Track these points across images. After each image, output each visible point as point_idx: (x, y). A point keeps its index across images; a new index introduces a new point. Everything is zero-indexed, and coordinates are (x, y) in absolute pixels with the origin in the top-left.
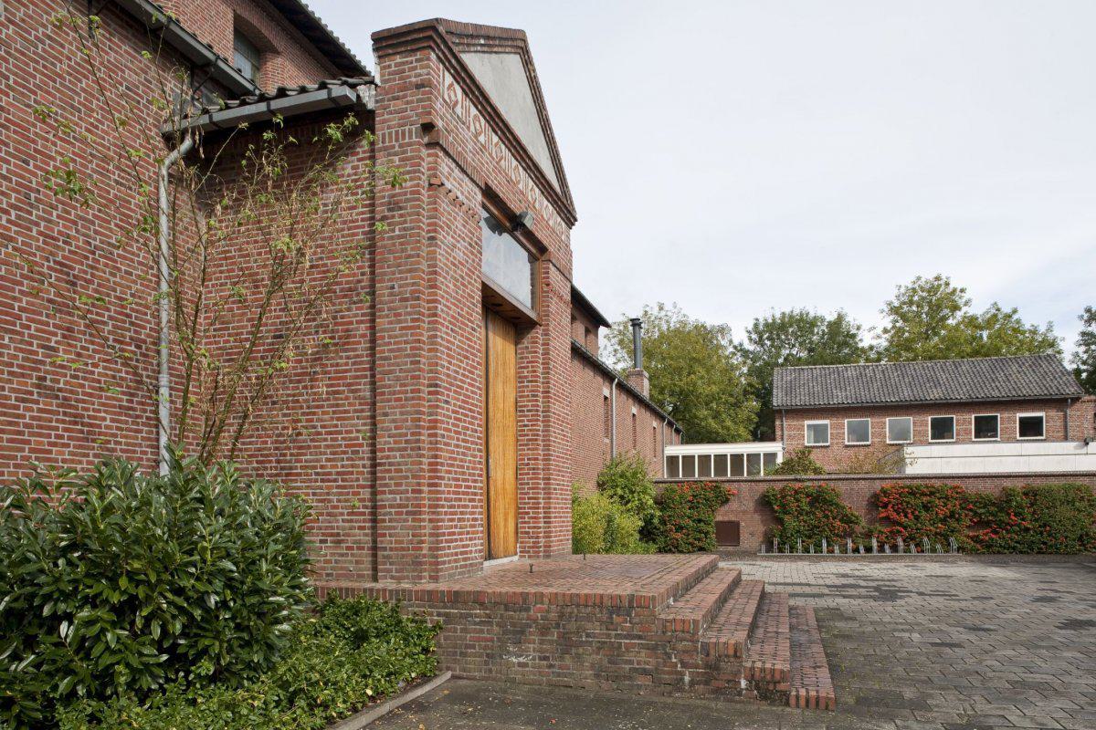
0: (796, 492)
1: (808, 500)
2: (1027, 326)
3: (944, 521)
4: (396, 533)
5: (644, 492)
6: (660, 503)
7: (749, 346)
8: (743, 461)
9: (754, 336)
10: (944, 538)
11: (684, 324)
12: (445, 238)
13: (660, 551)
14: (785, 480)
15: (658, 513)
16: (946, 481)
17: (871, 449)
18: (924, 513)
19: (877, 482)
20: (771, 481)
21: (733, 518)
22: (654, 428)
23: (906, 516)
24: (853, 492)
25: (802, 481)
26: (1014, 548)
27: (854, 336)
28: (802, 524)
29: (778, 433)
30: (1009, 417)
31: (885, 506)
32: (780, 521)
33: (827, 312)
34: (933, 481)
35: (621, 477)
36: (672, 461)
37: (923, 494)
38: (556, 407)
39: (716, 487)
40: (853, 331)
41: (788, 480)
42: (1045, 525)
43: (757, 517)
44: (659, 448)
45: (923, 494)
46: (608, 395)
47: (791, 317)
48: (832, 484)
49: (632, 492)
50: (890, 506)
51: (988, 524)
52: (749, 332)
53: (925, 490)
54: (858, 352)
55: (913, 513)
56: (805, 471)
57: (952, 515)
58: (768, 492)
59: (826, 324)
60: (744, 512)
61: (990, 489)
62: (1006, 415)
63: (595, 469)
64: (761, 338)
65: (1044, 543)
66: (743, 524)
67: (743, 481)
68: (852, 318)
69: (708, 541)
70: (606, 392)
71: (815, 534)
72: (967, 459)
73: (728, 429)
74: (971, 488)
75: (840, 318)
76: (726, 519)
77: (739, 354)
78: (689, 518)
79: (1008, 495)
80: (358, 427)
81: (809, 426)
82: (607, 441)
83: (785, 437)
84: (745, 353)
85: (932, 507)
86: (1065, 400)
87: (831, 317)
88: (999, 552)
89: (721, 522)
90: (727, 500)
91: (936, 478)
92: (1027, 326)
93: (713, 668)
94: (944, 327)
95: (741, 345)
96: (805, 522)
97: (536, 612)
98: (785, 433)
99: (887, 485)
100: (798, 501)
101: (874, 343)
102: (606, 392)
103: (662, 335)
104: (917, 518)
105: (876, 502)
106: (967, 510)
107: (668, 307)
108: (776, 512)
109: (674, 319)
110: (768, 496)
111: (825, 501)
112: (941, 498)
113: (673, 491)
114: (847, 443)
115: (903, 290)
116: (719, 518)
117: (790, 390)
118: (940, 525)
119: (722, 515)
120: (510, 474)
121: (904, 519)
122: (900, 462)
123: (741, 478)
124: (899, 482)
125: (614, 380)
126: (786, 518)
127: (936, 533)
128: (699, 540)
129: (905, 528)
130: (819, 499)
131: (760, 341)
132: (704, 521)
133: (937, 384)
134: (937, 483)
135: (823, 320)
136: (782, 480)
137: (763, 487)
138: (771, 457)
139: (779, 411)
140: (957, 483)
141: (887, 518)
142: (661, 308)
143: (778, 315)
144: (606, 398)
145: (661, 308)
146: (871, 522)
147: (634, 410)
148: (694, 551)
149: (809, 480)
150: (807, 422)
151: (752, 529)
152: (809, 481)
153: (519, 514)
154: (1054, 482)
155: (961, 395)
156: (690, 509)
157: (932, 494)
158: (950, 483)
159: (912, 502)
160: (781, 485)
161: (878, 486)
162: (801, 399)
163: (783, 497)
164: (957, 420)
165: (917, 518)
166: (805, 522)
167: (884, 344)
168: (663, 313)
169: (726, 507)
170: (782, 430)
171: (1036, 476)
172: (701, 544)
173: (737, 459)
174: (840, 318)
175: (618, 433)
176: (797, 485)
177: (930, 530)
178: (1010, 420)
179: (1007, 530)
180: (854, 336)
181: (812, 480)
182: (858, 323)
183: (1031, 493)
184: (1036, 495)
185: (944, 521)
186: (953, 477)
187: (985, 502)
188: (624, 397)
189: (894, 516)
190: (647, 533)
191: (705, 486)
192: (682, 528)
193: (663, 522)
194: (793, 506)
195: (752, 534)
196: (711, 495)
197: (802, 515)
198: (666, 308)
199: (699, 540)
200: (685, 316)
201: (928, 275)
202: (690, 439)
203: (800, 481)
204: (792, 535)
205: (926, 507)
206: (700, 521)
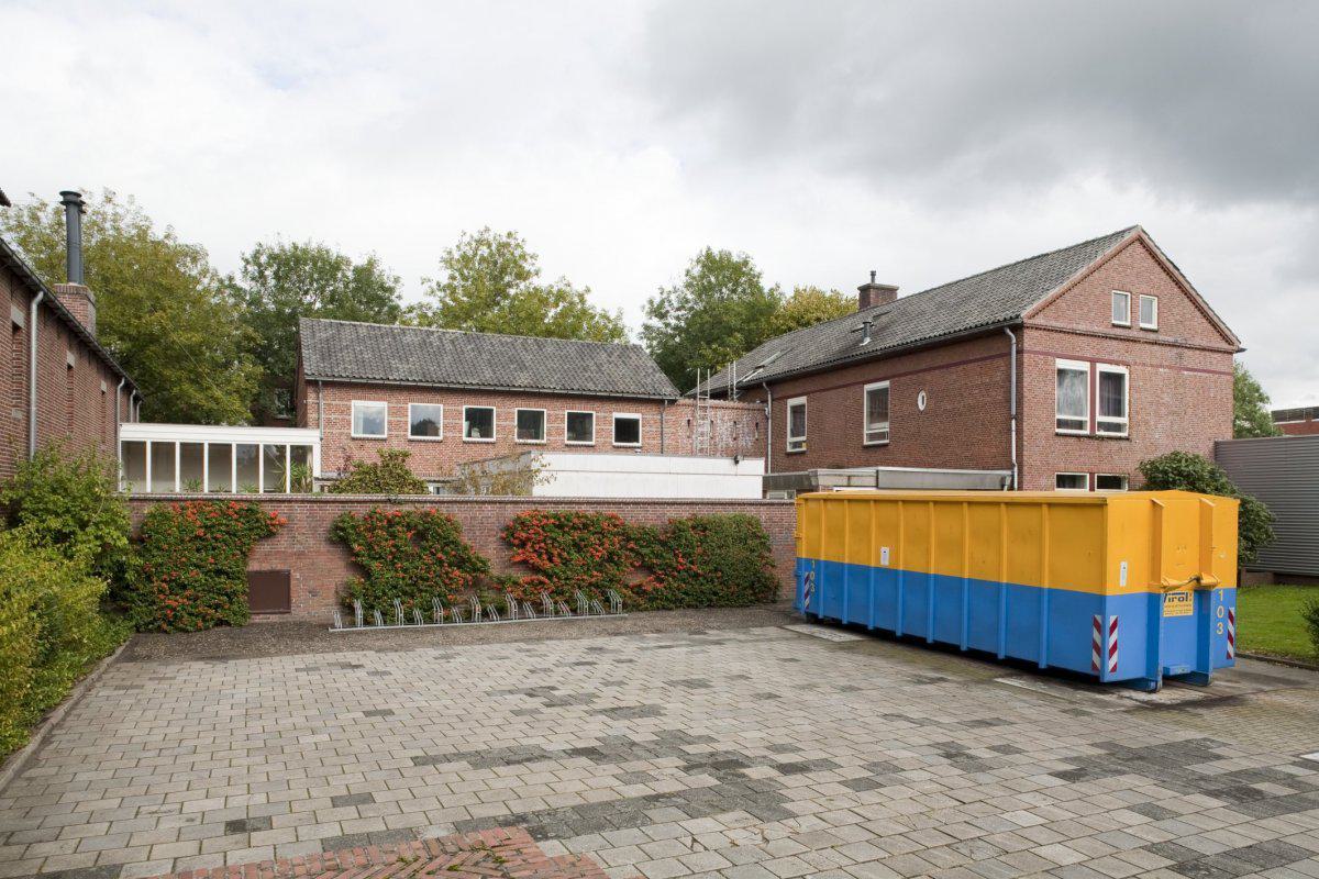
0: (391, 523)
1: (409, 535)
2: (599, 310)
3: (600, 567)
6: (140, 540)
7: (240, 282)
8: (202, 450)
9: (252, 268)
10: (600, 591)
11: (143, 233)
14: (371, 501)
16: (599, 508)
17: (442, 446)
18: (575, 556)
20: (347, 502)
21: (277, 565)
22: (103, 393)
23: (551, 560)
24: (475, 523)
25: (400, 503)
26: (681, 601)
27: (391, 290)
28: (401, 574)
29: (312, 416)
30: (605, 417)
31: (523, 544)
33: (353, 250)
34: (584, 507)
35: (54, 491)
37: (574, 528)
39: (249, 511)
40: (389, 284)
41: (377, 502)
42: (716, 570)
44: (110, 427)
45: (574, 528)
46: (21, 323)
47: (305, 251)
48: (444, 509)
49: (83, 525)
50: (530, 544)
52: (247, 262)
53: (576, 520)
54: (394, 314)
55: (559, 555)
57: (610, 558)
58: (343, 521)
59: (351, 268)
61: (649, 519)
62: (601, 414)
64: (261, 274)
65: (715, 594)
66: (296, 575)
67: (283, 501)
68: (387, 269)
69: (235, 607)
70: (17, 315)
71: (421, 591)
72: (609, 475)
73: (217, 401)
74: (632, 518)
75: (371, 263)
76: (266, 567)
77: (227, 291)
78: (197, 566)
79: (676, 530)
82: (20, 415)
83: (322, 423)
84: (238, 292)
85: (585, 546)
86: (662, 401)
87: (358, 260)
88: (664, 608)
89: (257, 572)
90: (270, 535)
91: (588, 503)
92: (599, 310)
94: (506, 296)
95: (231, 279)
96: (405, 571)
99: (523, 511)
100: (393, 536)
101: (425, 300)
102: (17, 315)
103: (104, 244)
104: (566, 562)
106: (627, 549)
107: (120, 199)
108: (357, 555)
109: (128, 220)
110: (343, 529)
112: (596, 533)
113: (165, 517)
114: (353, 435)
115: (467, 239)
117: (326, 354)
118: (595, 573)
121: (548, 565)
122: (528, 475)
123: (279, 496)
124: (540, 507)
125: (35, 295)
127: (590, 584)
128: (217, 607)
129: (549, 577)
130: (429, 532)
131: (260, 277)
132: (227, 574)
133: (522, 367)
134: (590, 511)
135: (348, 263)
136: (365, 502)
137: (332, 513)
138: (301, 454)
139: (314, 383)
140: (613, 510)
141: (525, 562)
143: (288, 246)
144: (16, 328)
145: (109, 200)
147: (71, 358)
148: (207, 629)
149: (407, 502)
152: (408, 504)
154: (721, 512)
155: (552, 384)
156: (198, 550)
157: (585, 526)
159: (560, 539)
160: (362, 511)
161: (511, 513)
162: (345, 369)
163: (372, 529)
164: (549, 415)
165: (566, 562)
166: (405, 571)
167: (436, 304)
168: (133, 208)
171: (702, 504)
172: (219, 615)
173: (221, 452)
174: (371, 263)
175: (40, 399)
176: (390, 510)
177: (583, 580)
178: (604, 420)
179: (674, 577)
180: (391, 290)
181: (413, 502)
182: (396, 274)
183: (701, 527)
184: (706, 529)
185: (600, 567)
186: (609, 503)
188: (51, 333)
189: (535, 559)
190: (116, 602)
191: (226, 508)
192: (184, 587)
195: (313, 593)
197: (400, 559)
198: (116, 200)
199: (217, 607)
200: (147, 219)
201: (499, 231)
202: (147, 417)
204: (385, 594)
205: (578, 547)
206: (219, 572)
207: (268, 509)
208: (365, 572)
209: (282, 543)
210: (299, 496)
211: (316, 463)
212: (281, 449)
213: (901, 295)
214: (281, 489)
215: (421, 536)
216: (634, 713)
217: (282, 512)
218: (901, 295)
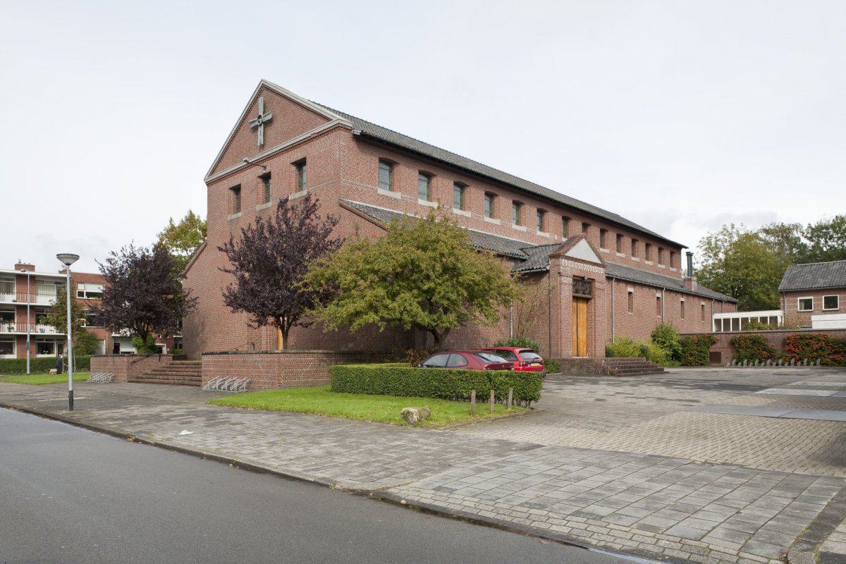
0: (746, 339)
4: (554, 349)
5: (672, 339)
12: (563, 292)
13: (683, 365)
15: (680, 348)
19: (786, 333)
21: (718, 350)
29: (782, 305)
32: (738, 352)
36: (718, 321)
38: (597, 319)
43: (729, 350)
48: (764, 335)
51: (839, 352)
56: (753, 328)
57: (821, 348)
60: (723, 348)
63: (652, 328)
74: (832, 336)
80: (547, 329)
81: (800, 300)
90: (715, 343)
93: (604, 370)
97: (577, 362)
98: (786, 304)
99: (789, 335)
105: (785, 342)
111: (758, 343)
116: (712, 351)
119: (713, 349)
120: (585, 336)
126: (741, 350)
129: (798, 355)
138: (774, 319)
140: (826, 333)
142: (733, 228)
145: (733, 228)
146: (784, 351)
150: (799, 298)
151: (726, 354)
153: (588, 346)
157: (811, 338)
158: (822, 333)
165: (803, 350)
169: (715, 346)
170: (784, 303)
185: (816, 351)
187: (836, 342)
193: (683, 352)
194: (743, 345)
196: (707, 340)
203: (749, 333)
205: (808, 345)
207: (715, 336)
208: (738, 352)
209: (718, 344)
210: (735, 332)
211: (779, 320)
212: (738, 319)
213: (202, 214)
214: (720, 330)
215: (754, 342)
216: (679, 477)
217: (718, 337)
218: (202, 214)
